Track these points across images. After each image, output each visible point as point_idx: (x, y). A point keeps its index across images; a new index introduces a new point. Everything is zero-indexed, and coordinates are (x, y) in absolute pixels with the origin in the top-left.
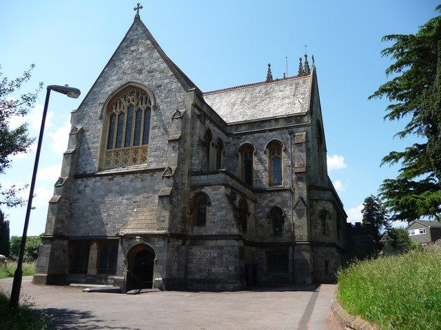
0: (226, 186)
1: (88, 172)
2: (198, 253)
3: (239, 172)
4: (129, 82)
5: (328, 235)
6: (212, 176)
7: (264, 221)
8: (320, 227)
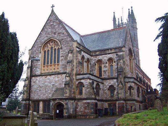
3: (96, 73)
8: (129, 93)
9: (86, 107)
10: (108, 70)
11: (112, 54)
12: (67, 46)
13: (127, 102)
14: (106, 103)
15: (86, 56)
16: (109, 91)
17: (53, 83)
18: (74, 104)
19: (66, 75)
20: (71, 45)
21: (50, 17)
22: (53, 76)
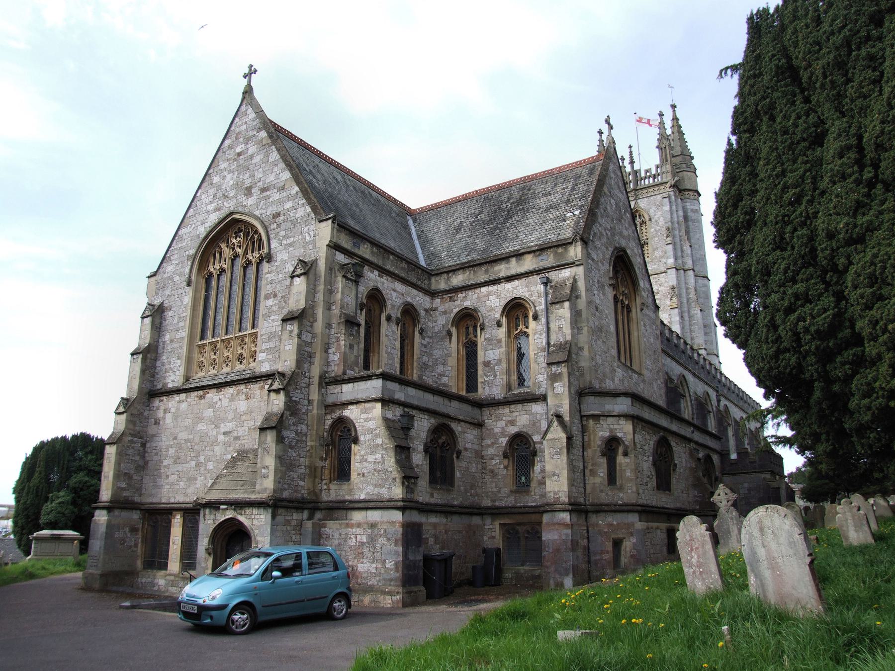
0: (386, 401)
1: (170, 385)
2: (336, 535)
4: (231, 214)
5: (621, 489)
6: (361, 385)
7: (498, 464)
8: (603, 473)
9: (362, 544)
10: (503, 357)
11: (524, 281)
12: (290, 245)
13: (593, 518)
14: (493, 520)
15: (396, 294)
16: (506, 462)
17: (229, 426)
18: (309, 525)
19: (271, 385)
20: (307, 238)
21: (237, 119)
22: (230, 390)
